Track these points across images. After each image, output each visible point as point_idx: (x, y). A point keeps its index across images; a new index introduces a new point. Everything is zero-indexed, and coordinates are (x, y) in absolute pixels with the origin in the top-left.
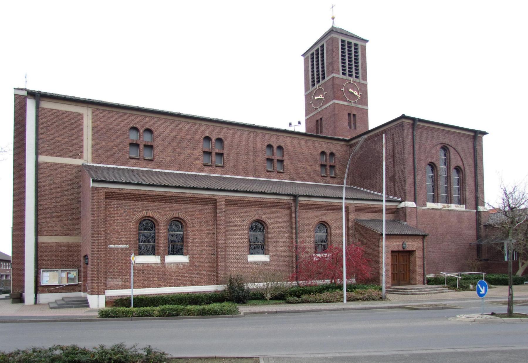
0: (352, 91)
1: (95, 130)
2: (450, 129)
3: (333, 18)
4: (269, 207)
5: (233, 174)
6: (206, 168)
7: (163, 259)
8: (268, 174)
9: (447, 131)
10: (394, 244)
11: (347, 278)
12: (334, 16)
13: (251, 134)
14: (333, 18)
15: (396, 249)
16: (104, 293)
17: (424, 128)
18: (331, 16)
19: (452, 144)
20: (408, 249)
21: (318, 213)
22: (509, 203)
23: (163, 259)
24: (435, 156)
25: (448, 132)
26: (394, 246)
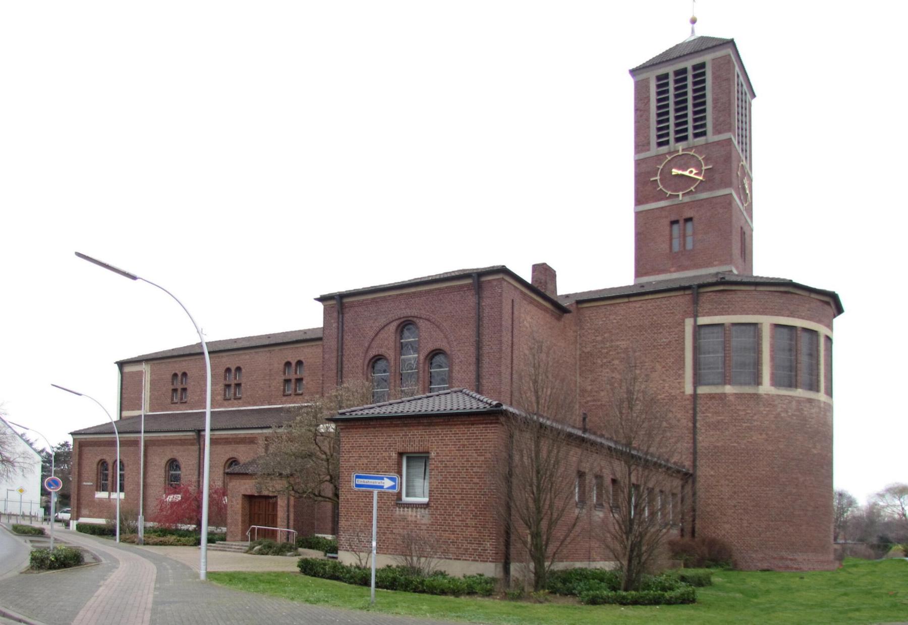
0: (680, 172)
1: (153, 383)
2: (413, 290)
3: (693, 21)
4: (181, 445)
5: (250, 405)
6: (226, 403)
7: (110, 495)
8: (285, 398)
9: (408, 294)
10: (247, 486)
11: (210, 523)
12: (696, 16)
13: (268, 355)
14: (693, 21)
15: (249, 493)
16: (77, 519)
17: (361, 304)
18: (690, 17)
19: (414, 312)
20: (265, 493)
21: (228, 448)
22: (630, 392)
23: (110, 495)
24: (386, 343)
25: (384, 299)
26: (246, 489)
